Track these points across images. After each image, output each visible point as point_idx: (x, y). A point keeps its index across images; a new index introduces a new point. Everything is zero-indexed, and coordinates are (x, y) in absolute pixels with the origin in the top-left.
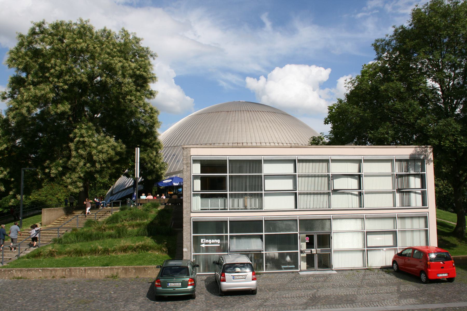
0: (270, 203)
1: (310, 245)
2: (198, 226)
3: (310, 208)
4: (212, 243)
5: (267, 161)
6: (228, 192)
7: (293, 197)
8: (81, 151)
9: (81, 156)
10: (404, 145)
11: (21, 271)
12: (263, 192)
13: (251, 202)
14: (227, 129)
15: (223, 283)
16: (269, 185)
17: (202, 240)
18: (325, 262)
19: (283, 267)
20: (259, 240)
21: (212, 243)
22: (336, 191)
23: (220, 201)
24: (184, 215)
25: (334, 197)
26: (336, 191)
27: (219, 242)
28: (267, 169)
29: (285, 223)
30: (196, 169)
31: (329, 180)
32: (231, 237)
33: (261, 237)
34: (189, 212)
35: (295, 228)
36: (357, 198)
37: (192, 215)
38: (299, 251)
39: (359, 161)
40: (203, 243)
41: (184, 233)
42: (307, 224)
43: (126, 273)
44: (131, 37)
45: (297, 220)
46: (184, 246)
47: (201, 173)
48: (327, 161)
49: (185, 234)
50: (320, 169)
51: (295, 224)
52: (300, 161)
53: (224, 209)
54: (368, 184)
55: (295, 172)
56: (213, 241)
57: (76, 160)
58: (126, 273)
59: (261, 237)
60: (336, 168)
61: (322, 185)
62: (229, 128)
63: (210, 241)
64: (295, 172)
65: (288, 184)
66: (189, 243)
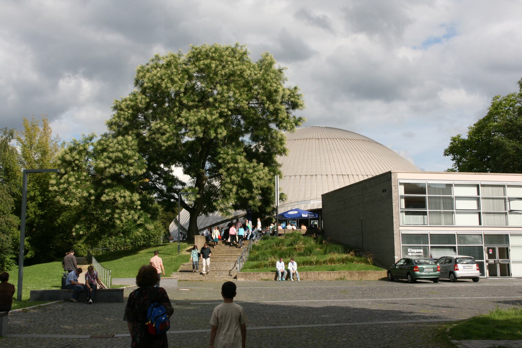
0: (460, 220)
1: (491, 256)
2: (408, 238)
3: (493, 227)
4: (417, 253)
5: (456, 185)
6: (428, 210)
7: (477, 215)
8: (234, 177)
9: (233, 182)
11: (267, 274)
12: (455, 211)
15: (457, 272)
16: (459, 205)
17: (409, 250)
18: (506, 271)
21: (417, 253)
22: (511, 211)
23: (420, 217)
24: (395, 229)
25: (510, 217)
26: (511, 211)
28: (457, 192)
30: (401, 190)
31: (505, 202)
32: (431, 247)
33: (454, 248)
34: (398, 226)
35: (480, 241)
37: (401, 228)
38: (484, 261)
41: (395, 244)
42: (490, 238)
43: (351, 276)
45: (481, 235)
46: (395, 254)
47: (405, 193)
48: (504, 186)
49: (395, 244)
50: (498, 192)
51: (481, 238)
52: (483, 186)
53: (424, 225)
55: (478, 194)
56: (418, 251)
57: (230, 186)
58: (351, 276)
59: (454, 248)
61: (499, 206)
63: (415, 251)
64: (478, 194)
65: (473, 205)
66: (399, 252)
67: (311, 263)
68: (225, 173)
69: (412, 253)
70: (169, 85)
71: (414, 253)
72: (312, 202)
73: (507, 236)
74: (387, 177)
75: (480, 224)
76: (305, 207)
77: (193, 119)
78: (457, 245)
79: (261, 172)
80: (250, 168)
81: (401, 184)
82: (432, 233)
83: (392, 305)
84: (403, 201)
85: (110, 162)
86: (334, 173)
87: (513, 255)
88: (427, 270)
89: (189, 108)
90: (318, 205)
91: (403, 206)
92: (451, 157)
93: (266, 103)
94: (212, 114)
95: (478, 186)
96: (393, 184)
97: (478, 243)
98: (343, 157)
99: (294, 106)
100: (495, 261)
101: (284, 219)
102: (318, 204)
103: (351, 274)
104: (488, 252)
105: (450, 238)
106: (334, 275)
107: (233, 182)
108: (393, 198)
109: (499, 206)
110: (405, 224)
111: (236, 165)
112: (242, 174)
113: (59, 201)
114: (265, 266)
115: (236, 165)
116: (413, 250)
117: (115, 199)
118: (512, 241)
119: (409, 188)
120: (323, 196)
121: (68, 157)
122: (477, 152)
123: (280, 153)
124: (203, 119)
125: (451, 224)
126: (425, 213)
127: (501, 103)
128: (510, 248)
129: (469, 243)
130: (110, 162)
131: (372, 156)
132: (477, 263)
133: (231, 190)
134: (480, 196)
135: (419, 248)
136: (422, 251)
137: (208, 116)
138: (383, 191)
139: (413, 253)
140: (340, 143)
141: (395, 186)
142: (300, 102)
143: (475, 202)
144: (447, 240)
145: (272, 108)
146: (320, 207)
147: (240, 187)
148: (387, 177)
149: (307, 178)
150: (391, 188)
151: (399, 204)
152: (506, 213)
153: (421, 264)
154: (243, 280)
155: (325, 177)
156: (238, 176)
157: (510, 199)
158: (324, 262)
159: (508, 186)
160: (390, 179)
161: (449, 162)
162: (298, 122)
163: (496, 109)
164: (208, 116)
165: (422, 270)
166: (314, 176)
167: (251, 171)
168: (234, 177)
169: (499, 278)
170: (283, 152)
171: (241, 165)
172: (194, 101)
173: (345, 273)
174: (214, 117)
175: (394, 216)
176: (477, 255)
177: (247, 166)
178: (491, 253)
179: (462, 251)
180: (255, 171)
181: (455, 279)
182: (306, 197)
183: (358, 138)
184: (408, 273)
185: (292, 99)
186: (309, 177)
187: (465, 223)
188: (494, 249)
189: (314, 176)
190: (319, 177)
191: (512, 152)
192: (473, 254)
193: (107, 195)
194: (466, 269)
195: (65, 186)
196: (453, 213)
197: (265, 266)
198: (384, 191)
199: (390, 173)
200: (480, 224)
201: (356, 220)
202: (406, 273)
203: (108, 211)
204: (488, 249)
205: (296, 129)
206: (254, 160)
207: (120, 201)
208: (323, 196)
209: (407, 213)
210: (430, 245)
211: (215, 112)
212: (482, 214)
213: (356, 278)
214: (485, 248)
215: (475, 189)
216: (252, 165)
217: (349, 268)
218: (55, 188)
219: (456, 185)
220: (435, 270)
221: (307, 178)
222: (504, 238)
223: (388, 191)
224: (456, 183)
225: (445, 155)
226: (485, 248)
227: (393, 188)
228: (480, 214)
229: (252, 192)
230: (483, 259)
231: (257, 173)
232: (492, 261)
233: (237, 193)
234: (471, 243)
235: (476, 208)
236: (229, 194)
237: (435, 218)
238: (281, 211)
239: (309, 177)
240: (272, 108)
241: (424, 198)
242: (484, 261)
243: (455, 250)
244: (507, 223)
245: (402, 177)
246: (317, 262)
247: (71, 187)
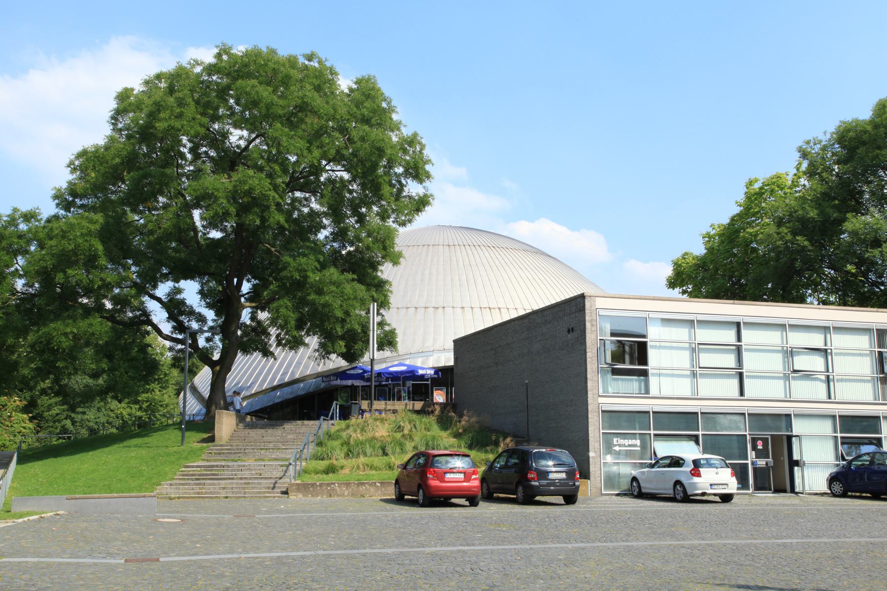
2: (613, 417)
7: (735, 382)
10: (778, 302)
13: (633, 384)
14: (452, 280)
19: (850, 494)
20: (692, 444)
21: (630, 446)
27: (639, 444)
29: (729, 417)
32: (655, 435)
33: (696, 439)
34: (596, 396)
35: (742, 426)
36: (824, 386)
37: (601, 400)
38: (749, 462)
39: (825, 329)
40: (615, 445)
44: (813, 214)
45: (744, 414)
49: (591, 429)
51: (743, 420)
54: (750, 362)
55: (739, 339)
56: (631, 442)
60: (798, 339)
62: (464, 278)
63: (626, 442)
64: (739, 339)
69: (620, 445)
71: (625, 446)
73: (788, 416)
75: (742, 393)
76: (423, 363)
78: (700, 433)
82: (656, 409)
83: (287, 390)
86: (476, 304)
90: (448, 360)
95: (738, 324)
96: (587, 318)
97: (738, 429)
100: (767, 464)
102: (447, 359)
104: (754, 448)
108: (588, 344)
116: (622, 442)
120: (455, 341)
122: (743, 266)
129: (722, 430)
131: (541, 277)
132: (733, 466)
136: (638, 442)
138: (569, 331)
140: (487, 255)
141: (591, 321)
146: (451, 363)
148: (575, 307)
150: (585, 325)
155: (459, 311)
160: (582, 309)
163: (754, 200)
166: (441, 310)
175: (589, 376)
176: (736, 451)
178: (760, 447)
182: (426, 345)
186: (431, 310)
189: (441, 310)
190: (449, 311)
198: (570, 330)
199: (582, 297)
208: (455, 341)
210: (652, 432)
223: (578, 331)
227: (588, 325)
228: (741, 376)
230: (747, 459)
232: (762, 463)
234: (726, 429)
239: (431, 310)
242: (749, 462)
243: (697, 443)
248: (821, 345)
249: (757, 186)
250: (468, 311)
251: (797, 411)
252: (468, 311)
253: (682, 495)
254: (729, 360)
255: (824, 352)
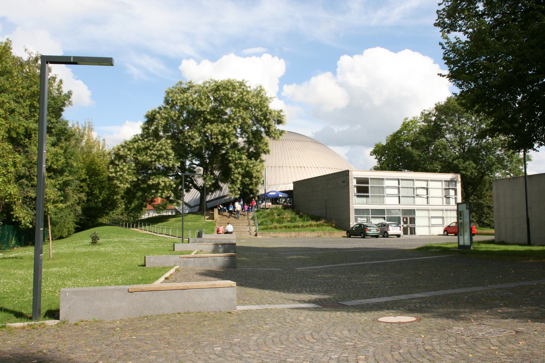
2: (357, 211)
3: (407, 204)
5: (387, 179)
6: (370, 195)
7: (398, 198)
16: (388, 191)
18: (413, 231)
33: (384, 218)
36: (426, 200)
42: (405, 212)
48: (413, 180)
50: (409, 184)
52: (402, 180)
55: (399, 185)
61: (410, 192)
64: (399, 185)
67: (298, 227)
68: (233, 167)
70: (200, 107)
72: (281, 186)
74: (346, 173)
75: (399, 203)
77: (216, 131)
78: (386, 216)
79: (258, 167)
80: (251, 164)
81: (354, 178)
84: (356, 188)
85: (156, 157)
87: (418, 222)
88: (373, 231)
89: (212, 123)
91: (356, 192)
92: (374, 156)
93: (263, 121)
94: (229, 128)
95: (399, 180)
97: (398, 214)
98: (277, 151)
99: (279, 122)
101: (265, 197)
102: (291, 187)
103: (325, 233)
104: (403, 221)
105: (382, 211)
106: (315, 234)
107: (239, 173)
109: (410, 192)
110: (356, 203)
111: (241, 162)
112: (245, 168)
113: (116, 184)
114: (271, 229)
115: (241, 162)
117: (159, 183)
118: (417, 213)
119: (360, 181)
121: (121, 153)
123: (265, 153)
124: (222, 130)
125: (383, 203)
126: (368, 196)
127: (408, 124)
128: (416, 218)
130: (156, 157)
133: (238, 178)
134: (400, 186)
135: (364, 217)
136: (366, 219)
137: (227, 129)
139: (362, 220)
142: (283, 120)
143: (397, 190)
144: (381, 212)
145: (266, 124)
146: (292, 189)
147: (244, 176)
148: (346, 173)
149: (281, 171)
151: (353, 191)
152: (414, 197)
153: (370, 227)
154: (261, 237)
156: (242, 169)
157: (417, 188)
158: (306, 226)
159: (417, 180)
161: (374, 161)
162: (282, 132)
163: (405, 126)
164: (227, 129)
165: (370, 230)
166: (281, 168)
167: (251, 166)
168: (240, 170)
169: (409, 236)
170: (267, 152)
171: (245, 162)
172: (214, 117)
173: (321, 233)
174: (230, 130)
177: (249, 162)
179: (390, 219)
180: (254, 166)
181: (388, 236)
183: (304, 140)
184: (362, 232)
185: (279, 118)
186: (277, 168)
187: (390, 203)
188: (407, 218)
189: (281, 168)
190: (284, 168)
191: (417, 158)
192: (397, 221)
193: (153, 180)
194: (393, 230)
195: (121, 173)
196: (384, 196)
197: (271, 229)
199: (348, 171)
200: (399, 203)
201: (320, 199)
202: (360, 231)
203: (153, 191)
204: (403, 218)
205: (281, 138)
206: (253, 158)
207: (163, 184)
209: (358, 196)
210: (370, 216)
211: (230, 126)
212: (401, 198)
213: (327, 235)
214: (402, 218)
215: (397, 182)
216: (252, 162)
217: (323, 230)
218: (114, 175)
219: (387, 179)
220: (377, 230)
221: (281, 171)
222: (413, 212)
224: (387, 177)
225: (371, 155)
226: (402, 218)
228: (399, 197)
229: (252, 180)
231: (255, 167)
232: (405, 226)
233: (241, 181)
235: (397, 193)
236: (236, 181)
237: (375, 200)
238: (261, 192)
239: (277, 168)
240: (266, 124)
241: (368, 187)
243: (385, 219)
244: (414, 203)
245: (355, 174)
246: (302, 226)
247: (125, 174)
248: (425, 186)
249: (408, 120)
250: (292, 168)
251: (418, 208)
252: (292, 168)
253: (233, 108)
254: (395, 191)
255: (443, 218)
